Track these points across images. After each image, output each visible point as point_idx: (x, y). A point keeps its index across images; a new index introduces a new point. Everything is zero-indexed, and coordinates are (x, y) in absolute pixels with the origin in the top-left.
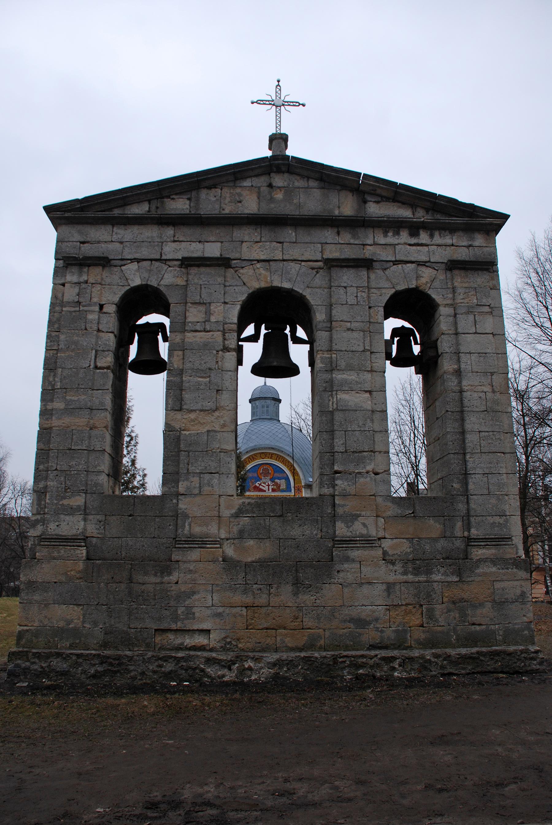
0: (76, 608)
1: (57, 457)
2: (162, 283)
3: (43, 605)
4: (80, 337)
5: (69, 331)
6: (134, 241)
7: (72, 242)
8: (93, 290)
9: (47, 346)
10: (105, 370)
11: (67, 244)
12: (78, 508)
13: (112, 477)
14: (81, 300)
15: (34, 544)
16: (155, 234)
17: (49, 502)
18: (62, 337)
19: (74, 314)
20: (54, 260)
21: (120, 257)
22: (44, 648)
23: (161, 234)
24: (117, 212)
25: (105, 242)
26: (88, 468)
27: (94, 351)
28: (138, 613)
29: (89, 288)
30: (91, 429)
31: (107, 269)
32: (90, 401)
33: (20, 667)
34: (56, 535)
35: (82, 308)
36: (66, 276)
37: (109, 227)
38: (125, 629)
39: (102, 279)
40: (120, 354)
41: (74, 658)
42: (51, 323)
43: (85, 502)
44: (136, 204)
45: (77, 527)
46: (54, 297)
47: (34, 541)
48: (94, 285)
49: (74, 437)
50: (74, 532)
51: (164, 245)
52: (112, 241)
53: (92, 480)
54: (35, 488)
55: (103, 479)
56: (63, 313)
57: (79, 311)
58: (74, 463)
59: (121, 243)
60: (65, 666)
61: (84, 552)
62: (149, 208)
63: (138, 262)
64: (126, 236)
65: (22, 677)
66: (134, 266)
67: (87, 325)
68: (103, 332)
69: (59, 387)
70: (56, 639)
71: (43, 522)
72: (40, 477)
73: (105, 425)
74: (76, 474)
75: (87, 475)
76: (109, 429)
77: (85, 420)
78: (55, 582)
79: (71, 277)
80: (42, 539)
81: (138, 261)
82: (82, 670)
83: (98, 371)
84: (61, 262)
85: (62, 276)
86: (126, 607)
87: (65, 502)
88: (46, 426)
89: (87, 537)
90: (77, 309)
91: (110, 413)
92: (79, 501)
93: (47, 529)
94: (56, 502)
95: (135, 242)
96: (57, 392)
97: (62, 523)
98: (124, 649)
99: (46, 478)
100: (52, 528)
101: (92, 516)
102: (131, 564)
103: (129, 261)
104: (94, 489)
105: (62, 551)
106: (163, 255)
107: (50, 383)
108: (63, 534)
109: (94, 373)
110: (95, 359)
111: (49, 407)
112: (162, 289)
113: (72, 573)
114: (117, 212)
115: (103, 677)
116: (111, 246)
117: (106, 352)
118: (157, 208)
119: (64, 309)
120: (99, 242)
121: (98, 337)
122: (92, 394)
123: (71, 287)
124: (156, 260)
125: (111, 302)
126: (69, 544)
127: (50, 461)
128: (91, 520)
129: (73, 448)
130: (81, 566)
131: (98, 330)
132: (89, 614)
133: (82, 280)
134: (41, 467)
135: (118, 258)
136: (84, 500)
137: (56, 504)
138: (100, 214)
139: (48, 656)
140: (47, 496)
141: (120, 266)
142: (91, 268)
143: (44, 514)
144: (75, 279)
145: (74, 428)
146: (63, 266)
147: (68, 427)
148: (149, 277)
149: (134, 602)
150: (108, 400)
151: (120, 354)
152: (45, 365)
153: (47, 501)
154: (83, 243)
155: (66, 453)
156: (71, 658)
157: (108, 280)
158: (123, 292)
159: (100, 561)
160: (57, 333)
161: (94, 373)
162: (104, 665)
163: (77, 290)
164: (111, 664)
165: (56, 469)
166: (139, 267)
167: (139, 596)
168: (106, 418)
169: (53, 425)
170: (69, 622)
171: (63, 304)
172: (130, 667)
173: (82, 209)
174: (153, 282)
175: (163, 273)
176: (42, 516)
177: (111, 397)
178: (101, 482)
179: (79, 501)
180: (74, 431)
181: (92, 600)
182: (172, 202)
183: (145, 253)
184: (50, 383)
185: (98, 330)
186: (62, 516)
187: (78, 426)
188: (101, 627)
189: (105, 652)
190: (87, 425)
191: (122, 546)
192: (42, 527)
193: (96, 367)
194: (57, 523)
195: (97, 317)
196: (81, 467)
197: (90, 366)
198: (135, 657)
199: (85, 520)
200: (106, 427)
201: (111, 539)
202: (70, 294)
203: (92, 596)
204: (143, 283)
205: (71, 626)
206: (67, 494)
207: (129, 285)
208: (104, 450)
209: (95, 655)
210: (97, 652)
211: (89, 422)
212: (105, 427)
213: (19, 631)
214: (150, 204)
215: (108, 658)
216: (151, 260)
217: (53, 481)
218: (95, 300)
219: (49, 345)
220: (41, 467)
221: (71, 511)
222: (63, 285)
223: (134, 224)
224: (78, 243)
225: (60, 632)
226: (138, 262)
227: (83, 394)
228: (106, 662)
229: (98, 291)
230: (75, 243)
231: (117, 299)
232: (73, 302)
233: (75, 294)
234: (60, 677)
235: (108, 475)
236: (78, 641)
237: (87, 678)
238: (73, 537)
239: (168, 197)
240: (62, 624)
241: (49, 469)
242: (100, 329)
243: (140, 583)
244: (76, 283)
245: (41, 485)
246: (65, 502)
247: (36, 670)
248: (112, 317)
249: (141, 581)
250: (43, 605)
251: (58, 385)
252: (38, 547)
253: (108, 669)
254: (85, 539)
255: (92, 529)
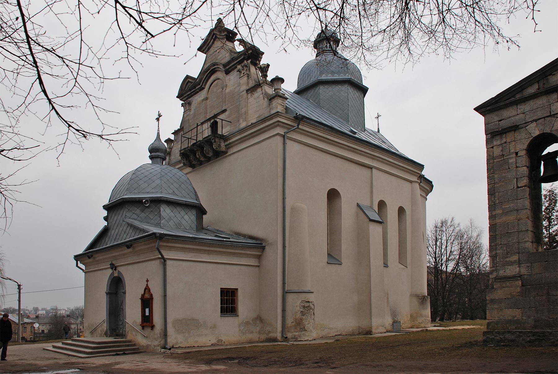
0: (517, 310)
1: (501, 238)
2: (553, 129)
3: (499, 310)
4: (507, 173)
5: (499, 172)
6: (532, 109)
7: (494, 122)
8: (510, 146)
9: (488, 183)
10: (524, 188)
11: (491, 124)
12: (515, 261)
13: (535, 242)
14: (504, 153)
15: (493, 282)
16: (545, 101)
17: (498, 260)
18: (496, 176)
19: (501, 162)
20: (485, 135)
21: (524, 122)
22: (502, 329)
23: (549, 100)
24: (518, 96)
25: (514, 116)
26: (518, 241)
27: (515, 179)
28: (554, 310)
29: (508, 145)
30: (519, 220)
31: (517, 131)
32: (516, 206)
33: (489, 338)
34: (504, 276)
35: (505, 158)
36: (493, 142)
37: (515, 107)
38: (547, 319)
39: (515, 138)
40: (533, 175)
41: (518, 333)
42: (488, 170)
43: (519, 258)
44: (530, 87)
45: (515, 271)
46: (488, 155)
47: (492, 280)
48: (510, 143)
49: (509, 226)
50: (514, 273)
51: (551, 106)
52: (518, 114)
53: (522, 247)
54: (491, 255)
55: (529, 245)
56: (495, 163)
57: (504, 159)
58: (510, 239)
59: (524, 113)
60: (513, 337)
61: (520, 283)
62: (539, 86)
63: (536, 121)
64: (526, 108)
65: (491, 343)
66: (534, 124)
67: (509, 166)
68: (520, 167)
69: (498, 202)
70: (508, 325)
71: (496, 270)
72: (492, 249)
73: (526, 217)
74: (512, 245)
75: (519, 244)
76: (530, 218)
77: (515, 216)
78: (505, 299)
79: (496, 142)
80: (497, 279)
81: (536, 121)
82: (523, 339)
83: (519, 189)
84: (489, 135)
85: (491, 143)
86: (546, 308)
87: (507, 259)
88: (492, 223)
89: (521, 275)
90: (503, 159)
91: (529, 210)
92: (515, 258)
93: (498, 274)
94: (502, 260)
95: (532, 110)
96: (497, 205)
97: (506, 270)
98: (547, 329)
99: (496, 249)
100: (501, 273)
101: (523, 264)
102: (548, 286)
103: (530, 123)
104: (524, 251)
105: (508, 284)
106: (552, 112)
107: (492, 201)
108: (507, 275)
109: (517, 191)
110: (517, 183)
111: (494, 214)
112: (553, 133)
113: (514, 293)
114: (518, 96)
115: (535, 342)
116: (517, 118)
117: (523, 178)
118: (544, 84)
119: (495, 161)
120: (510, 117)
121: (516, 171)
122: (517, 202)
123: (497, 148)
124: (547, 117)
125: (522, 149)
126: (511, 279)
127: (497, 241)
128: (523, 267)
129: (509, 232)
130: (519, 289)
131: (517, 166)
132: (525, 313)
133: (503, 142)
134: (493, 244)
135: (523, 123)
136: (518, 257)
137: (502, 261)
138: (507, 102)
139: (503, 333)
140: (497, 257)
141: (525, 127)
142: (507, 134)
143: (497, 267)
144: (499, 143)
145: (508, 222)
146: (491, 138)
147: (506, 222)
148: (544, 128)
149: (551, 305)
150: (527, 203)
151: (533, 175)
152: (488, 193)
153: (498, 260)
154: (500, 121)
155: (505, 235)
156: (516, 333)
157: (519, 138)
158: (529, 142)
159: (530, 286)
160: (493, 175)
161: (517, 191)
162: (535, 336)
163: (501, 148)
164: (539, 336)
165: (501, 244)
166: (537, 124)
167: (554, 302)
168: (527, 213)
169: (497, 222)
170: (514, 317)
171: (494, 158)
172: (550, 337)
173: (496, 102)
174: (547, 130)
175: (553, 123)
176: (495, 268)
177: (529, 201)
178: (527, 247)
179: (515, 258)
180: (509, 223)
181: (526, 306)
182: (553, 77)
183: (539, 114)
184: (492, 201)
185: (517, 166)
186: (506, 266)
187: (511, 220)
188: (532, 318)
189: (535, 330)
190: (516, 219)
191: (542, 277)
192: (496, 273)
193: (518, 187)
194: (504, 271)
195: (515, 160)
196: (514, 241)
197: (514, 188)
198: (553, 332)
199: (519, 267)
200: (528, 218)
201: (536, 275)
202: (497, 151)
203: (526, 304)
204: (541, 133)
205: (515, 319)
206: (508, 255)
207: (532, 137)
208: (528, 230)
209: (529, 332)
210: (531, 330)
211: (517, 217)
212: (527, 218)
213: (488, 322)
214: (538, 83)
215: (537, 333)
216: (544, 118)
217: (500, 250)
218: (512, 151)
219: (489, 182)
220: (493, 244)
221: (512, 263)
222: (493, 148)
223: (530, 99)
224: (498, 122)
225: (510, 322)
226: (536, 121)
227: (512, 203)
228: (536, 335)
229: (513, 145)
230: (495, 122)
231: (525, 146)
232: (500, 155)
233: (500, 151)
234: (510, 342)
235: (532, 242)
236: (519, 326)
237: (526, 343)
238: (514, 276)
239: (551, 74)
240: (510, 318)
241: (497, 244)
242: (518, 166)
243: (555, 295)
244: (499, 145)
245: (494, 253)
246: (507, 259)
247: (497, 339)
248: (524, 157)
249: (555, 294)
250: (499, 310)
251: (497, 201)
252: (495, 283)
253: (537, 339)
254: (520, 276)
255: (524, 271)
